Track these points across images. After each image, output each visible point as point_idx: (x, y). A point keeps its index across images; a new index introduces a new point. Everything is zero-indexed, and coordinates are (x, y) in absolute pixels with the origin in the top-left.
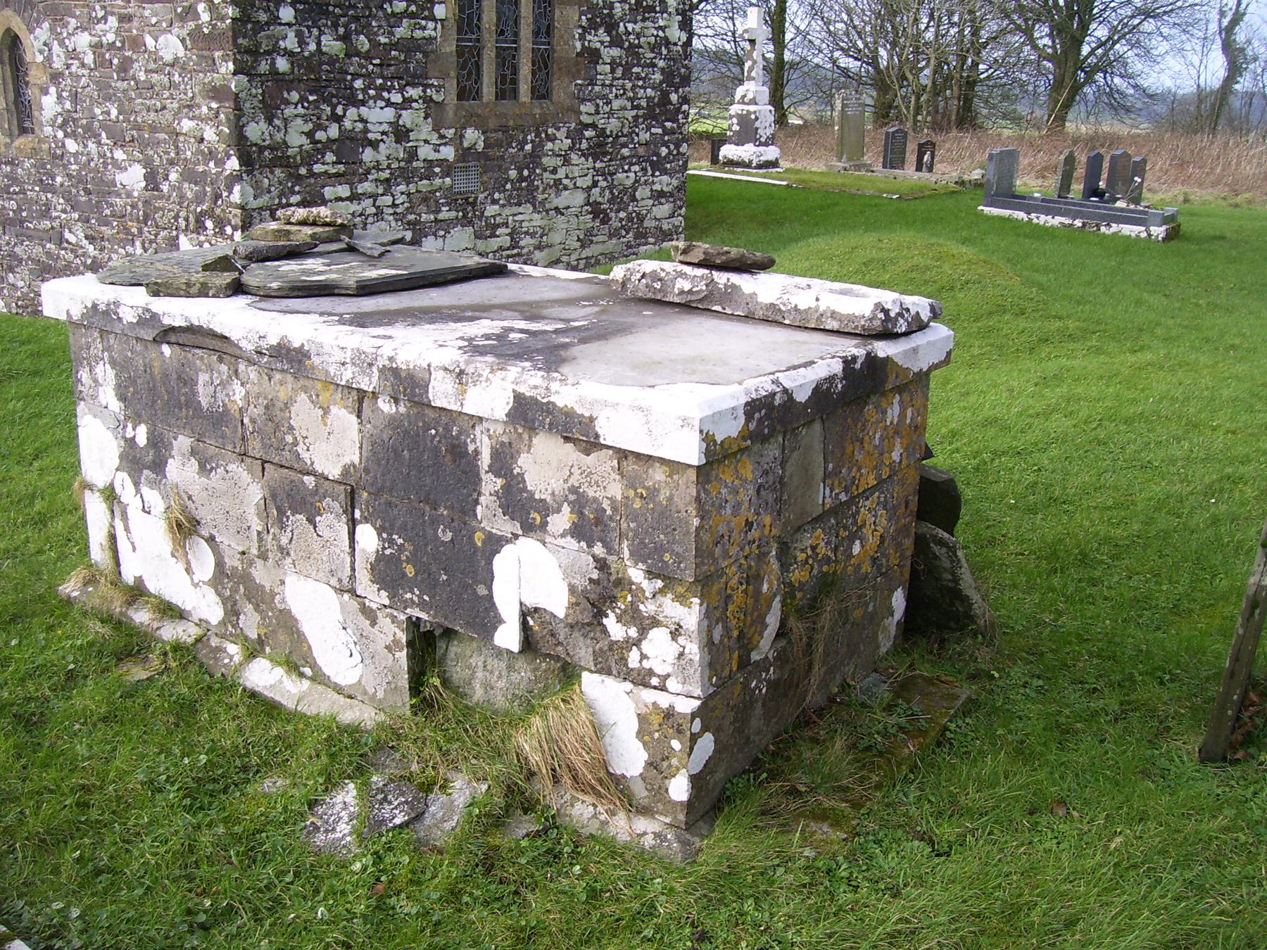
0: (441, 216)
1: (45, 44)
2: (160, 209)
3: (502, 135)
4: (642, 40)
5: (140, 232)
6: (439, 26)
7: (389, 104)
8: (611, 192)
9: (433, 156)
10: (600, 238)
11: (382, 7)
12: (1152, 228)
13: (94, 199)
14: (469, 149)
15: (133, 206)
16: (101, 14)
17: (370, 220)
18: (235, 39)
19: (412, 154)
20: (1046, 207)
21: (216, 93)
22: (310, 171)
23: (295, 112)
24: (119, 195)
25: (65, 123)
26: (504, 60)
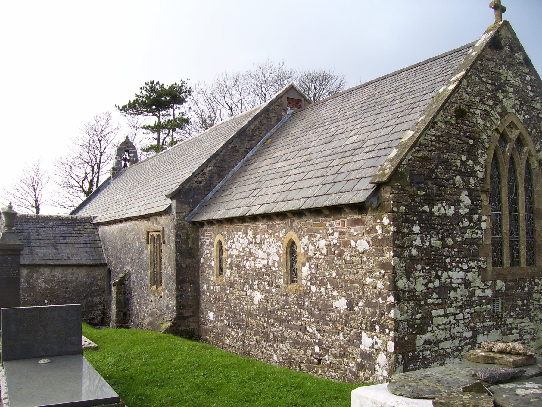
0: (486, 324)
1: (306, 245)
2: (353, 319)
3: (514, 283)
5: (343, 329)
6: (484, 232)
7: (462, 269)
9: (482, 294)
11: (458, 224)
13: (322, 313)
14: (499, 290)
15: (340, 317)
16: (331, 231)
17: (453, 326)
18: (394, 241)
19: (472, 294)
21: (384, 266)
22: (426, 302)
23: (420, 274)
24: (334, 312)
25: (312, 279)
26: (513, 247)
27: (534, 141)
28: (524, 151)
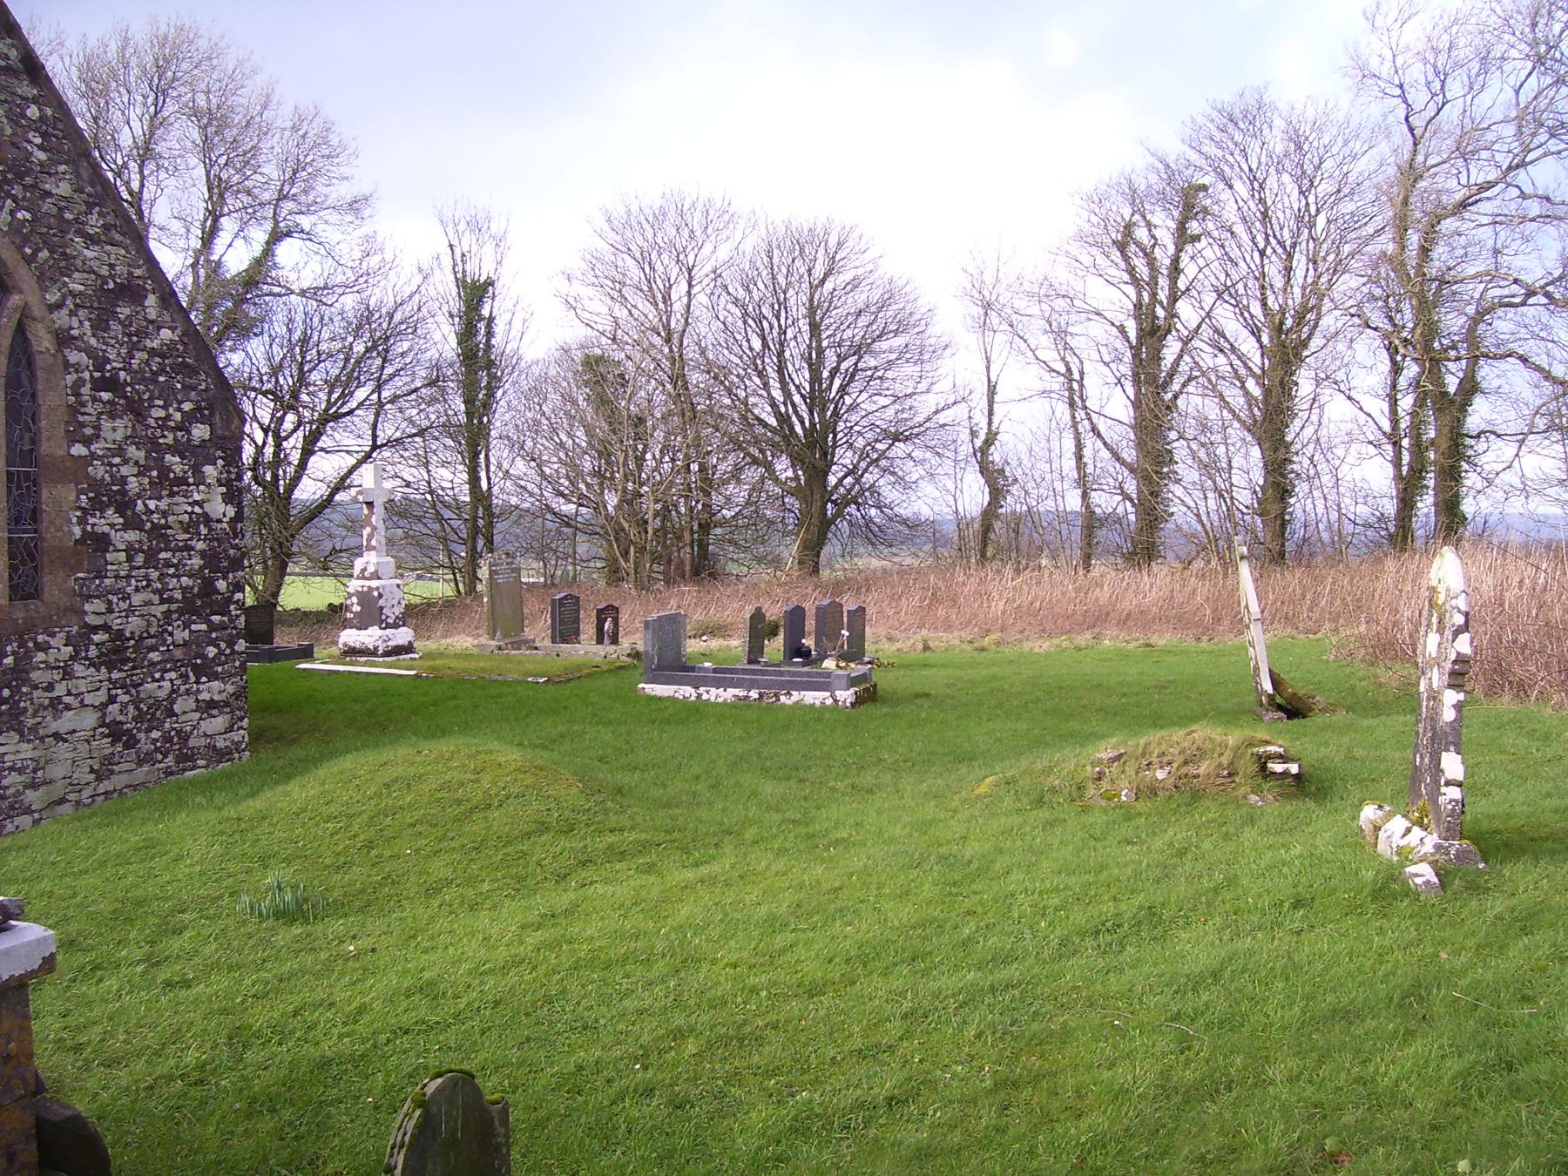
4: (171, 519)
8: (137, 708)
10: (125, 767)
12: (838, 693)
20: (722, 677)
27: (40, 279)
28: (9, 304)
